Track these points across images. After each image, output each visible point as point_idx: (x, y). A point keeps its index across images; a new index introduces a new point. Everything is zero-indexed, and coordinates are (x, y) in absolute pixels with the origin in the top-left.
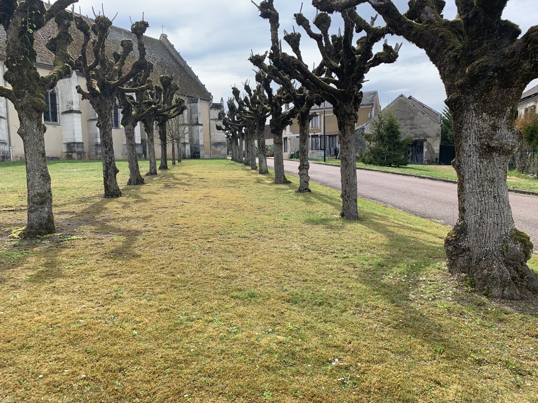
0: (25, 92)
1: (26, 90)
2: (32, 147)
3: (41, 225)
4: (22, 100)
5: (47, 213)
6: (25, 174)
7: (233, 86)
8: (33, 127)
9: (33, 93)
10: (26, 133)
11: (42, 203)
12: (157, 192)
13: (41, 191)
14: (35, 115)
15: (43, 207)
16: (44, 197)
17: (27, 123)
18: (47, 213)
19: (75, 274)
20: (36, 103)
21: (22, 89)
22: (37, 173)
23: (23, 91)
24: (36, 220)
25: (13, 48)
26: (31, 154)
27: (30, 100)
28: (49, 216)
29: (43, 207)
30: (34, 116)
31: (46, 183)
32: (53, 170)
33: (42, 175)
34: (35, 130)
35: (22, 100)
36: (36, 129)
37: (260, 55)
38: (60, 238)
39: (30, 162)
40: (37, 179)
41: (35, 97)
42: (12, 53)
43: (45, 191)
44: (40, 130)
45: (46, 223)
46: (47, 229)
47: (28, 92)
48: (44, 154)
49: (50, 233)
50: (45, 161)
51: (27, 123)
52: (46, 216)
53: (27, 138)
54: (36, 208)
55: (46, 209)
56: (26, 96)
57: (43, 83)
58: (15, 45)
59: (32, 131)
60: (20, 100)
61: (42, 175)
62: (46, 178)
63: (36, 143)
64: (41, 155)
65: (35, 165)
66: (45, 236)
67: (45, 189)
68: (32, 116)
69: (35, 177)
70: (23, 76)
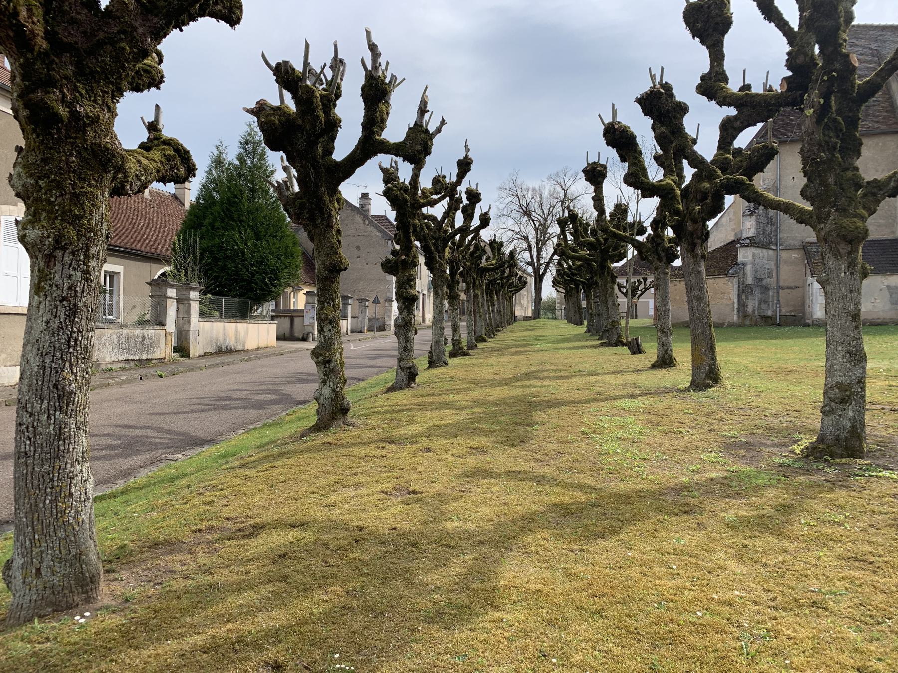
0: (829, 212)
1: (832, 207)
2: (836, 303)
3: (837, 439)
4: (825, 226)
5: (850, 420)
6: (823, 348)
7: (474, 187)
8: (840, 269)
9: (844, 210)
10: (828, 280)
11: (843, 401)
12: (471, 386)
13: (844, 380)
14: (843, 248)
15: (844, 409)
16: (847, 390)
17: (831, 263)
18: (850, 420)
19: (801, 538)
20: (845, 228)
21: (826, 208)
22: (840, 349)
23: (826, 210)
24: (831, 429)
25: (809, 144)
26: (833, 315)
27: (835, 224)
28: (853, 427)
29: (844, 409)
30: (841, 250)
31: (855, 366)
32: (871, 344)
33: (848, 352)
34: (843, 274)
35: (825, 226)
36: (845, 273)
37: (706, 72)
38: (861, 469)
39: (830, 329)
40: (840, 359)
41: (848, 217)
42: (808, 151)
43: (851, 381)
44: (852, 274)
45: (846, 437)
46: (846, 448)
47: (836, 211)
48: (855, 316)
49: (849, 456)
50: (857, 327)
51: (831, 263)
52: (849, 424)
53: (829, 288)
54: (833, 409)
55: (850, 413)
56: (832, 217)
57: (875, 191)
58: (811, 139)
59: (838, 276)
60: (822, 226)
61: (848, 352)
62: (858, 357)
63: (843, 297)
64: (850, 318)
65: (838, 334)
66: (838, 460)
67: (850, 376)
68: (838, 251)
69: (835, 355)
70: (827, 186)
